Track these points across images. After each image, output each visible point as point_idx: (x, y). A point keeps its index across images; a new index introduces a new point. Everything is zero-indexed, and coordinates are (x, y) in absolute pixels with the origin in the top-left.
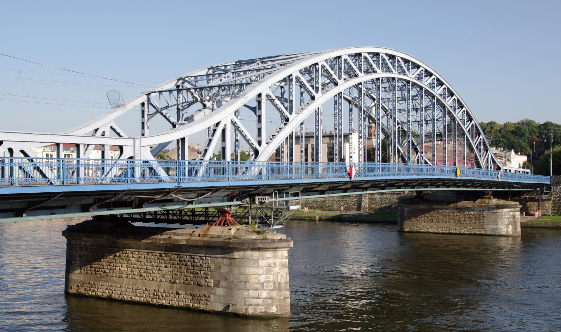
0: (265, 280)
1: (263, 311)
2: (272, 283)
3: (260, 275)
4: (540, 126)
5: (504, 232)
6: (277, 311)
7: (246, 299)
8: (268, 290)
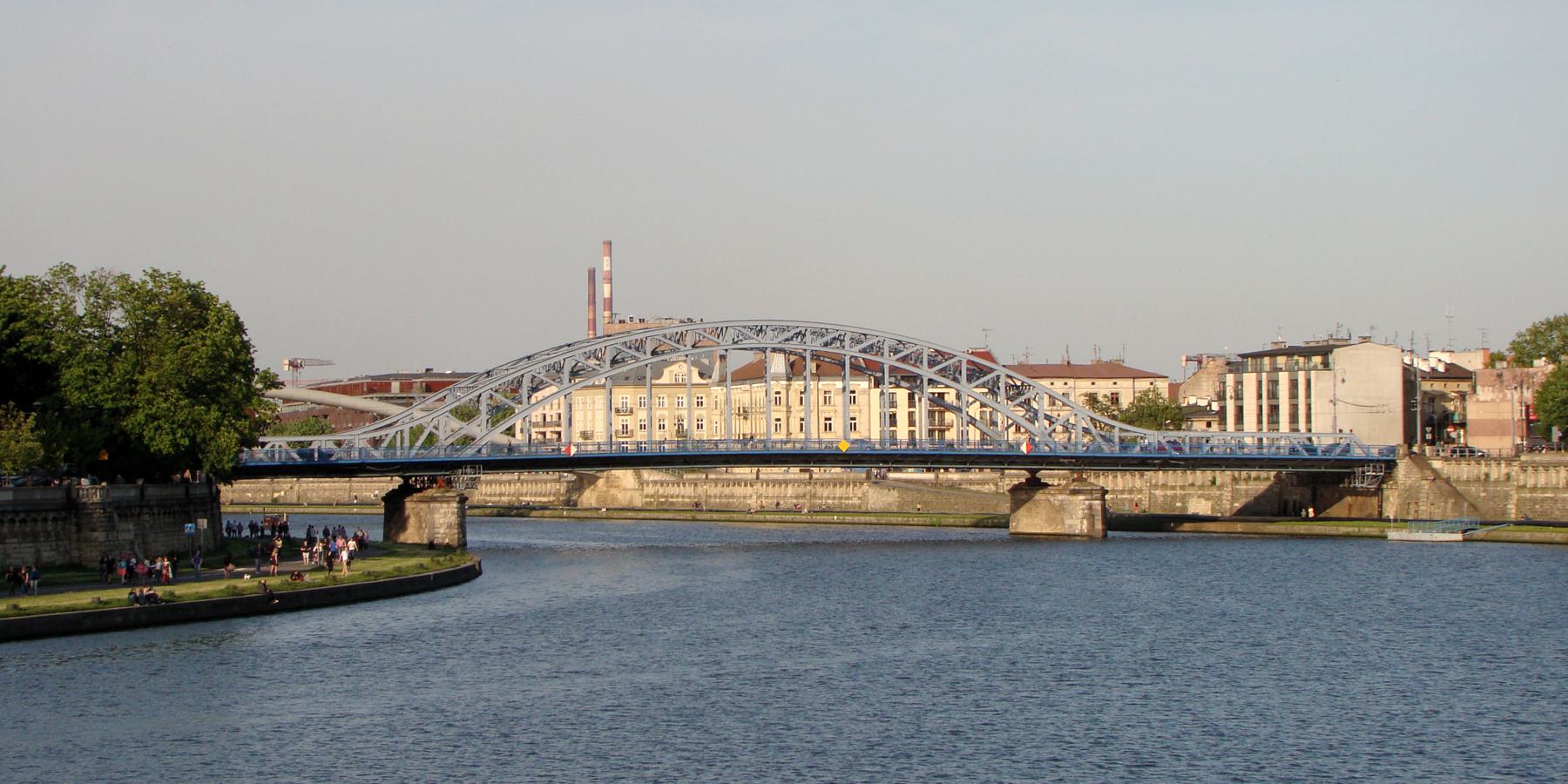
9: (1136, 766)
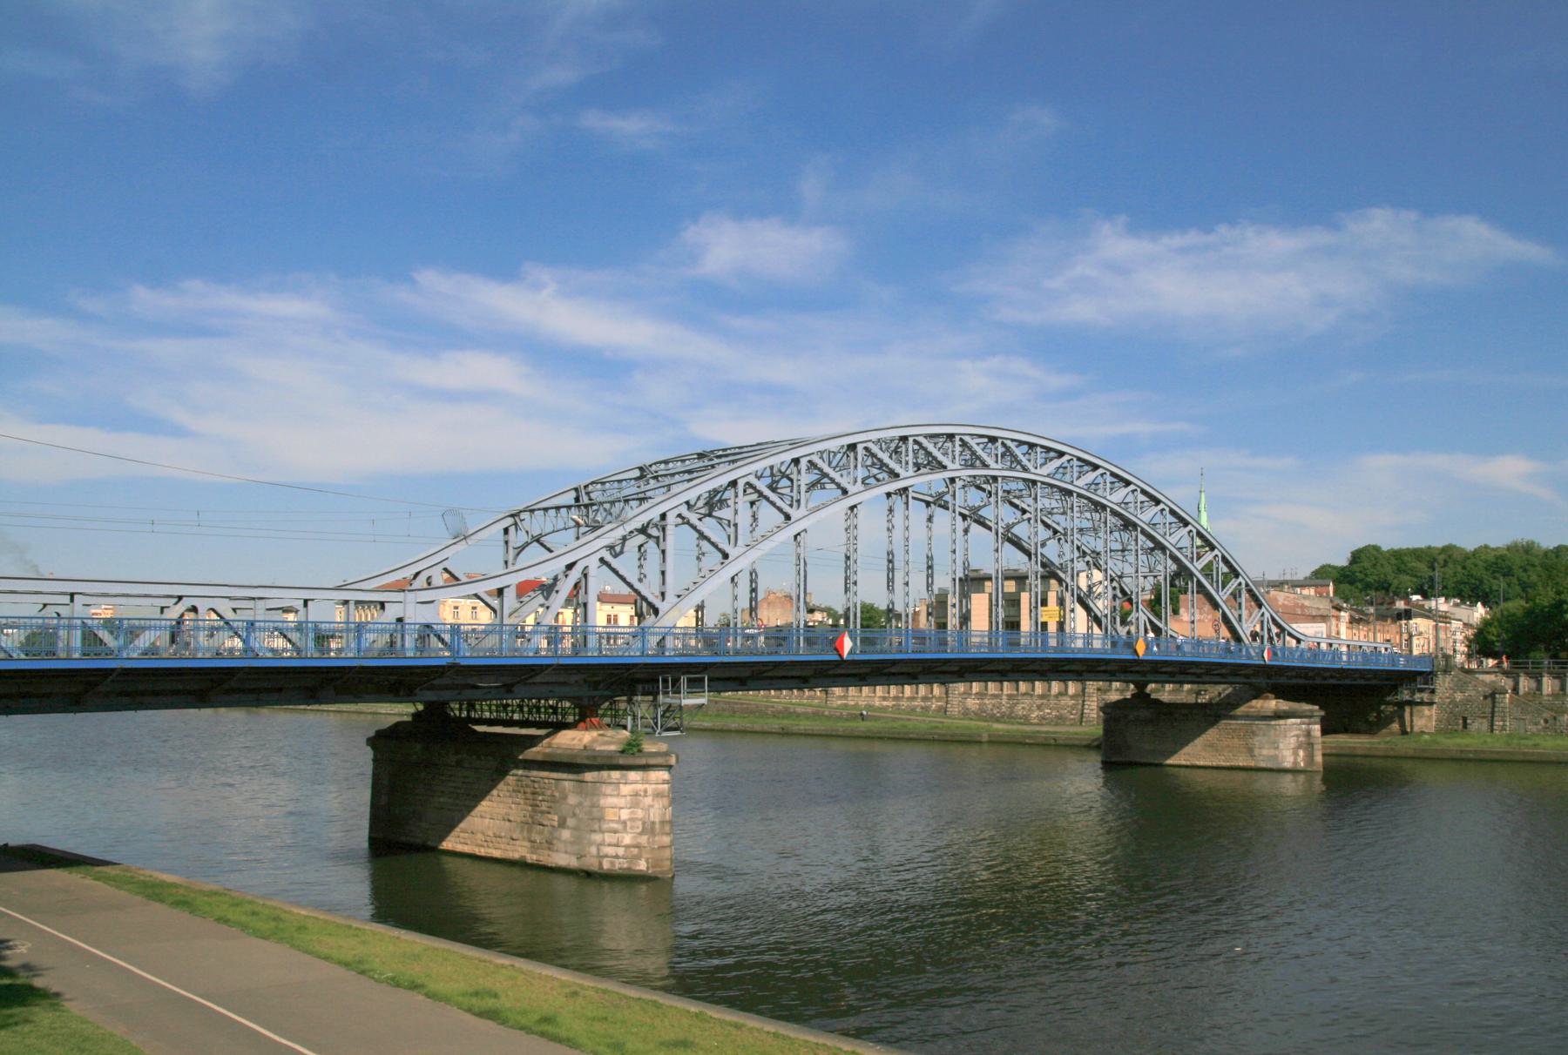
1: (625, 866)
4: (1546, 553)
5: (1288, 763)
6: (648, 868)
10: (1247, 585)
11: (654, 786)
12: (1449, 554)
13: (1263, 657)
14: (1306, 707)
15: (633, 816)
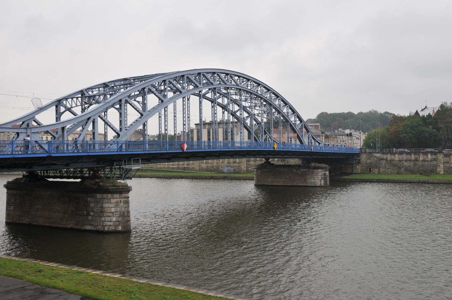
0: (115, 211)
1: (114, 229)
2: (119, 213)
3: (112, 208)
6: (122, 229)
7: (104, 222)
8: (117, 217)
9: (290, 277)
10: (304, 125)
11: (123, 199)
12: (350, 115)
13: (311, 149)
14: (324, 165)
15: (116, 210)
